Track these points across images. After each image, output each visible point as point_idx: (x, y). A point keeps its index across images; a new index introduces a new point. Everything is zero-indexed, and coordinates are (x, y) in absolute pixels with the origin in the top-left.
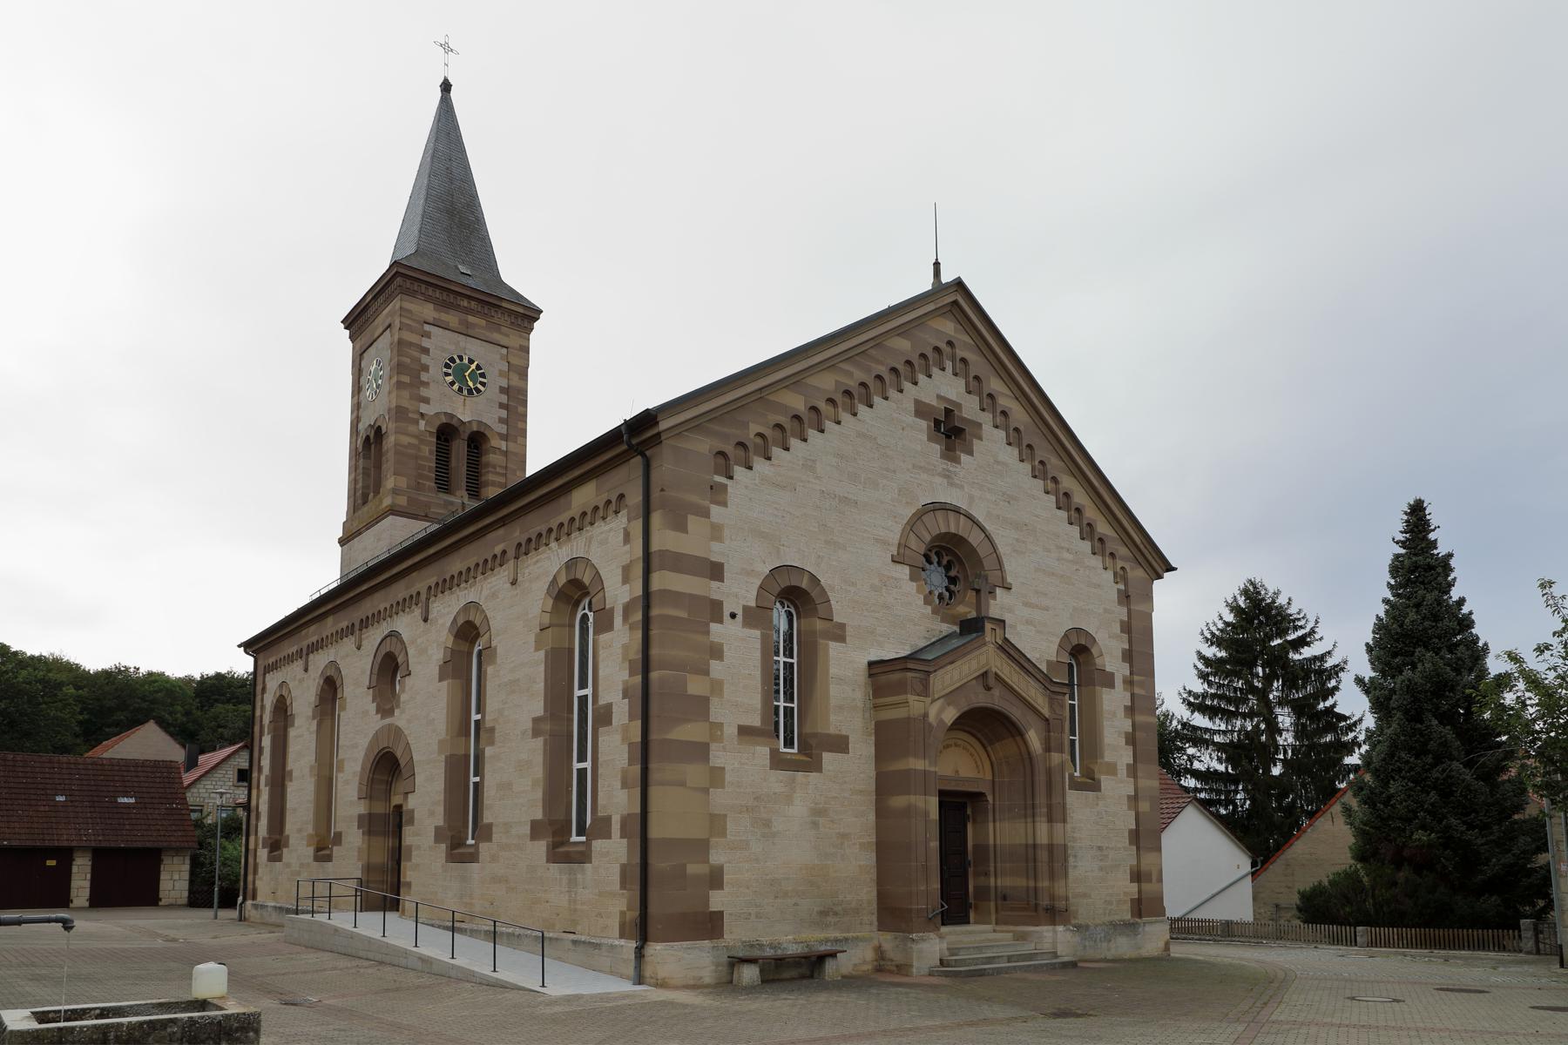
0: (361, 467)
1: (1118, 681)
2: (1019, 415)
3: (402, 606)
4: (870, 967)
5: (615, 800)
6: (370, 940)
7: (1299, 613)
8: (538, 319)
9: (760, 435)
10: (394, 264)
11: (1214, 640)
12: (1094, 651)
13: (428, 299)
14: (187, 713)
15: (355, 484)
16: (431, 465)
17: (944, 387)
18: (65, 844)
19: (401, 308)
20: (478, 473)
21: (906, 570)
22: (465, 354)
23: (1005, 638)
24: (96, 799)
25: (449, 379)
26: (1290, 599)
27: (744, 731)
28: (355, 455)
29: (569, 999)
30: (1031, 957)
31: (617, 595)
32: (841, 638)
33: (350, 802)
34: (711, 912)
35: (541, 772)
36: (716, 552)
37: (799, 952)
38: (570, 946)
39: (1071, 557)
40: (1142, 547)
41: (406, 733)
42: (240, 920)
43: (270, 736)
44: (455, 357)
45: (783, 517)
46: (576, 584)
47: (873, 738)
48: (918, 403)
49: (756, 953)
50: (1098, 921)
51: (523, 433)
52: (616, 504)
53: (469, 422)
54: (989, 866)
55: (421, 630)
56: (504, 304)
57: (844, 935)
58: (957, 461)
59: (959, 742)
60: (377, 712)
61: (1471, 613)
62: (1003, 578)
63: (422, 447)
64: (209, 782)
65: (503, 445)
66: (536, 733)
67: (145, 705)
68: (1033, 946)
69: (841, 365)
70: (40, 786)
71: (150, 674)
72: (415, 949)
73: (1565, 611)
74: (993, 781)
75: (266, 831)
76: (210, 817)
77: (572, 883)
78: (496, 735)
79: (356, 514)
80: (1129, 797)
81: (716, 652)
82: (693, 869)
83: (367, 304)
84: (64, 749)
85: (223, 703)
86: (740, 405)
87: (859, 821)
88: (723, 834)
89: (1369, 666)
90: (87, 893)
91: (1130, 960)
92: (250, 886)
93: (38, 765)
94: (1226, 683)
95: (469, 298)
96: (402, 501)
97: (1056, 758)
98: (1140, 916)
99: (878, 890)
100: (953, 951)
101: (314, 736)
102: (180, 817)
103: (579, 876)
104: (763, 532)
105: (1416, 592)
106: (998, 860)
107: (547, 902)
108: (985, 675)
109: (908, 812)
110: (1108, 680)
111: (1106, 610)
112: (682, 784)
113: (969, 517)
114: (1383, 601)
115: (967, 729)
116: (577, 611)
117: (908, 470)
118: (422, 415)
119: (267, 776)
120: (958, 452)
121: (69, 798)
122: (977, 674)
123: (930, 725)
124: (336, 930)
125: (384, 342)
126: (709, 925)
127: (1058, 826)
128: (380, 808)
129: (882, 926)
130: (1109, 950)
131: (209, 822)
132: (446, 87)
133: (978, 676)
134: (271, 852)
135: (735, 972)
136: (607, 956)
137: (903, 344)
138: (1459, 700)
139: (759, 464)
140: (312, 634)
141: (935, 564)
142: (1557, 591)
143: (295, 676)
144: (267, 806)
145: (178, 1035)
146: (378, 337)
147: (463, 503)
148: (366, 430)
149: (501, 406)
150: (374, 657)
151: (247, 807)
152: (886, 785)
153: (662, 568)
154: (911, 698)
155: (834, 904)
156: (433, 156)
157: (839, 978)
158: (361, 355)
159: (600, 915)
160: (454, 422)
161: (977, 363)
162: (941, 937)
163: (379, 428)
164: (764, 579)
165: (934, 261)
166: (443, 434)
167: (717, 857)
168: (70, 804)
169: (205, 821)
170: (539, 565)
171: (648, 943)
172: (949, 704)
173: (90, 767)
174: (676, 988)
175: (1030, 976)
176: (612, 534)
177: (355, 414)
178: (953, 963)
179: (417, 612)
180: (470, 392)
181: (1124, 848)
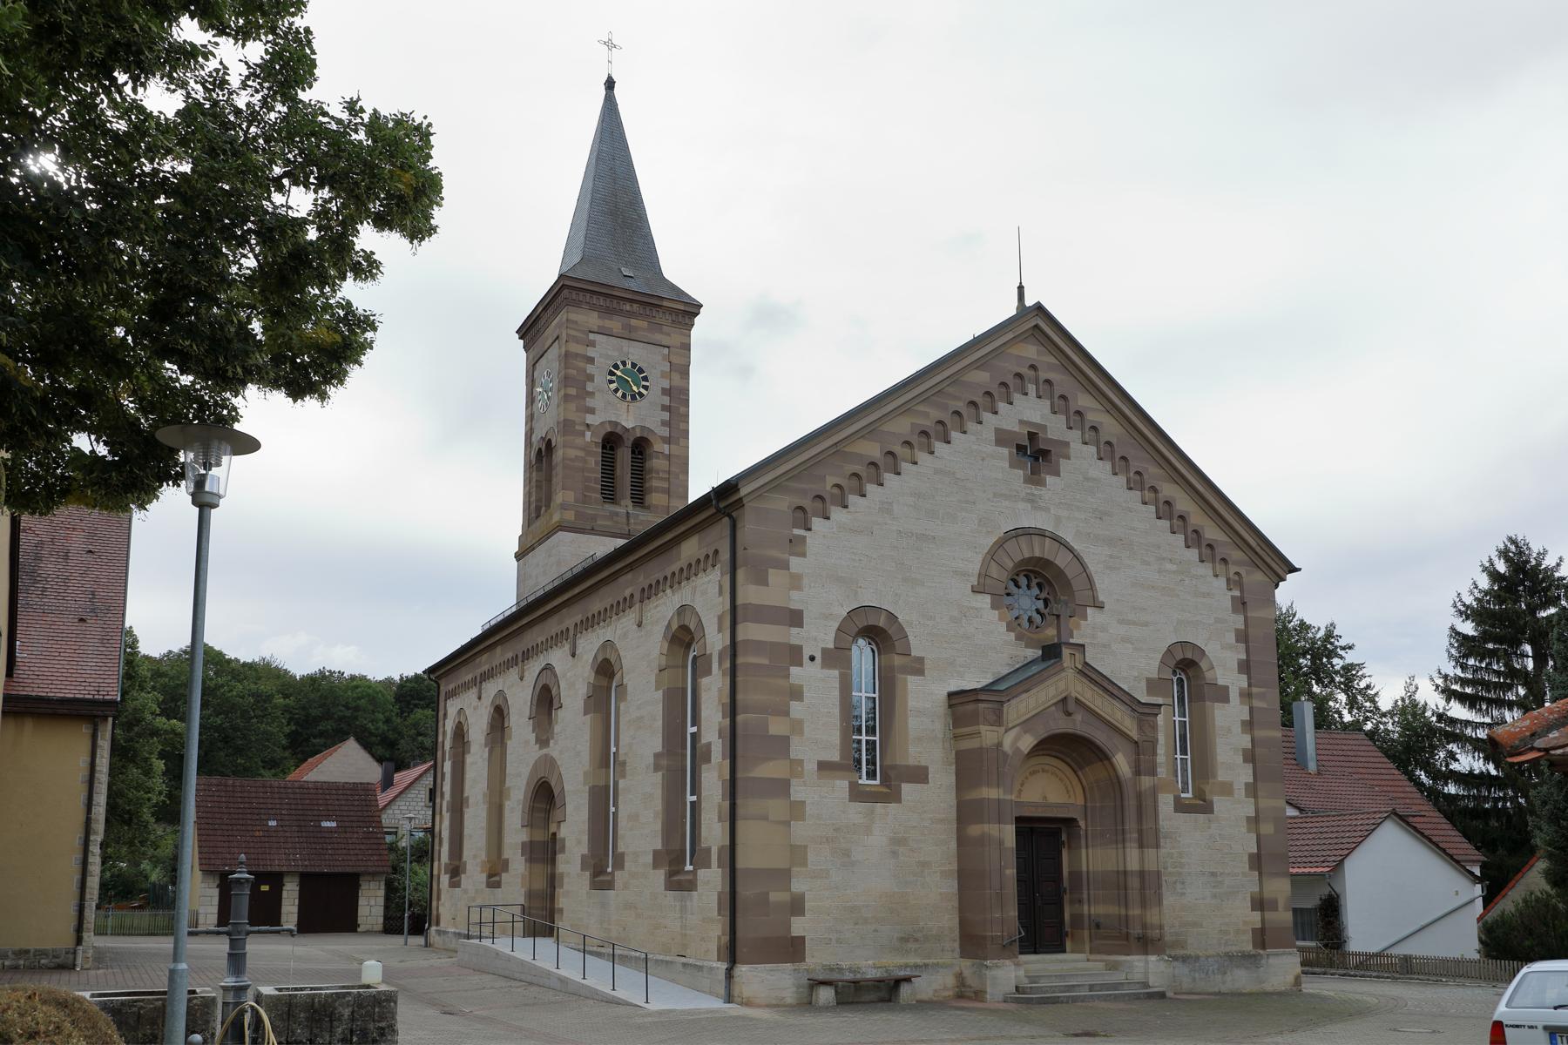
0: (534, 480)
1: (1234, 695)
2: (1111, 427)
3: (556, 640)
4: (951, 993)
5: (713, 833)
6: (522, 963)
8: (693, 325)
9: (838, 486)
10: (561, 276)
11: (1466, 613)
12: (1203, 665)
13: (593, 308)
14: (388, 721)
17: (1029, 410)
18: (277, 869)
19: (567, 320)
20: (642, 479)
21: (987, 599)
23: (1086, 663)
24: (303, 823)
25: (613, 386)
27: (824, 766)
28: (529, 467)
29: (661, 1013)
30: (1116, 986)
33: (516, 833)
34: (793, 937)
36: (796, 600)
37: (878, 976)
39: (1174, 567)
40: (1258, 549)
41: (559, 763)
42: (426, 946)
43: (450, 762)
44: (619, 363)
45: (860, 560)
46: (684, 628)
47: (954, 767)
48: (998, 431)
49: (835, 976)
50: (1211, 952)
51: (685, 434)
52: (711, 559)
54: (1082, 893)
56: (665, 303)
57: (923, 961)
58: (1042, 483)
59: (1047, 767)
60: (536, 743)
62: (1094, 598)
63: (589, 458)
64: (404, 803)
65: (666, 449)
66: (657, 768)
67: (348, 713)
68: (1124, 976)
69: (915, 408)
70: (256, 811)
71: (353, 678)
72: (533, 962)
74: (1085, 806)
76: (404, 840)
77: (683, 909)
78: (627, 768)
79: (532, 527)
80: (1248, 818)
81: (797, 694)
82: (776, 896)
83: (538, 316)
84: (272, 764)
85: (423, 708)
86: (816, 461)
87: (939, 849)
88: (804, 864)
90: (294, 918)
91: (1250, 994)
92: (434, 912)
93: (253, 789)
94: (1483, 665)
95: (632, 301)
96: (570, 516)
97: (1146, 781)
98: (1264, 948)
99: (960, 917)
100: (1033, 979)
102: (376, 841)
103: (688, 903)
104: (841, 577)
106: (1091, 887)
108: (1064, 700)
109: (982, 840)
110: (1222, 695)
111: (1217, 620)
112: (765, 818)
113: (1056, 539)
115: (1054, 754)
116: (689, 652)
117: (988, 499)
120: (1042, 475)
121: (280, 822)
122: (1055, 700)
123: (1005, 754)
124: (497, 954)
125: (554, 353)
126: (793, 949)
127: (1150, 853)
128: (540, 836)
129: (964, 954)
130: (1224, 983)
131: (404, 845)
132: (610, 84)
133: (1059, 702)
134: (451, 878)
135: (814, 994)
136: (707, 978)
137: (982, 377)
139: (837, 513)
140: (484, 663)
141: (1025, 588)
143: (471, 704)
144: (448, 831)
145: (352, 1003)
146: (548, 348)
147: (628, 513)
149: (664, 408)
150: (534, 688)
151: (430, 831)
152: (967, 813)
153: (745, 620)
154: (983, 728)
155: (914, 931)
156: (598, 158)
157: (914, 1002)
158: (534, 365)
159: (703, 939)
160: (618, 430)
162: (1017, 965)
163: (550, 440)
164: (842, 621)
166: (608, 443)
167: (797, 886)
168: (281, 829)
169: (399, 844)
170: (659, 609)
172: (1025, 732)
173: (298, 791)
174: (759, 1006)
175: (1103, 1005)
178: (1028, 990)
180: (633, 398)
181: (1243, 873)
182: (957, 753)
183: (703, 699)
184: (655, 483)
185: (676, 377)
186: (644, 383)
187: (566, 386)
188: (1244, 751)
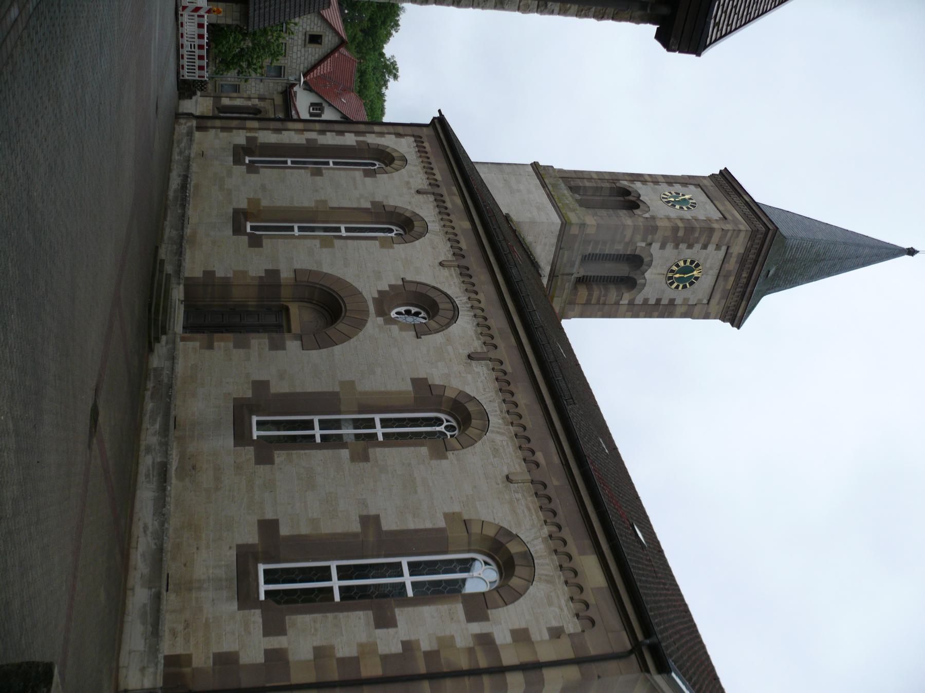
3: (483, 325)
13: (747, 250)
16: (607, 250)
22: (702, 275)
25: (681, 264)
28: (614, 177)
31: (501, 624)
35: (327, 531)
41: (361, 334)
51: (636, 315)
53: (645, 278)
55: (461, 351)
56: (744, 303)
60: (380, 292)
65: (625, 301)
75: (266, 141)
96: (574, 230)
101: (355, 205)
107: (198, 549)
118: (650, 244)
119: (316, 140)
132: (911, 252)
147: (572, 274)
148: (636, 191)
149: (658, 301)
160: (644, 267)
170: (527, 513)
176: (557, 610)
177: (648, 179)
179: (476, 345)
183: (440, 607)
185: (683, 309)
186: (681, 286)
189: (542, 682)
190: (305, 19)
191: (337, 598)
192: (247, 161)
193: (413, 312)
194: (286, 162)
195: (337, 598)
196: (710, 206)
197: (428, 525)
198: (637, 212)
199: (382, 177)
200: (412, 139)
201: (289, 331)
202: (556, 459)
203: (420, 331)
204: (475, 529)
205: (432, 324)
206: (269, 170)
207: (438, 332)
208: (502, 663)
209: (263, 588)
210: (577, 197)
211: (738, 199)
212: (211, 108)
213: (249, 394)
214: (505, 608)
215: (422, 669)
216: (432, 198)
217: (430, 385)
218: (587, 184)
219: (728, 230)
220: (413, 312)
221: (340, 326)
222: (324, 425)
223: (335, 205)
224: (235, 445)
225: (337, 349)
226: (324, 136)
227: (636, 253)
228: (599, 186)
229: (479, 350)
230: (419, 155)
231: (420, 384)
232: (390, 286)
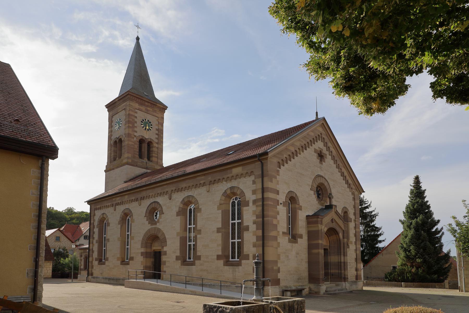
2: (334, 153)
3: (160, 194)
7: (366, 200)
13: (137, 102)
15: (110, 154)
22: (147, 119)
23: (337, 210)
25: (142, 126)
26: (364, 196)
27: (284, 233)
32: (301, 210)
35: (221, 242)
38: (235, 287)
40: (357, 185)
41: (162, 230)
48: (315, 149)
58: (322, 164)
61: (430, 205)
65: (157, 145)
73: (468, 208)
74: (330, 246)
87: (304, 256)
89: (403, 217)
95: (148, 102)
96: (130, 161)
105: (417, 199)
107: (224, 276)
113: (325, 178)
114: (409, 201)
119: (96, 240)
120: (322, 162)
126: (277, 282)
132: (138, 39)
138: (428, 226)
142: (466, 203)
147: (146, 162)
148: (115, 139)
149: (156, 134)
152: (311, 247)
160: (144, 138)
161: (327, 140)
165: (316, 112)
171: (265, 287)
177: (110, 133)
179: (166, 197)
182: (308, 231)
184: (154, 155)
187: (128, 124)
188: (354, 234)
189: (268, 188)
190: (49, 242)
191: (240, 240)
192: (104, 261)
193: (156, 214)
194: (105, 249)
195: (240, 240)
196: (120, 114)
197: (221, 215)
198: (123, 139)
199: (110, 221)
200: (96, 211)
201: (161, 250)
202: (203, 177)
203: (162, 213)
204: (222, 202)
205: (159, 209)
206: (107, 254)
207: (162, 208)
208: (260, 198)
209: (236, 259)
210: (117, 159)
211: (117, 103)
212: (85, 271)
213: (180, 261)
214: (246, 196)
215: (261, 219)
216: (117, 206)
217: (179, 211)
218: (112, 155)
219: (129, 108)
220: (156, 214)
221: (159, 235)
222: (190, 241)
223: (119, 235)
224: (195, 266)
225: (167, 237)
226: (95, 238)
227: (138, 141)
228: (113, 151)
229: (168, 196)
230: (101, 209)
231: (178, 214)
232: (147, 220)
